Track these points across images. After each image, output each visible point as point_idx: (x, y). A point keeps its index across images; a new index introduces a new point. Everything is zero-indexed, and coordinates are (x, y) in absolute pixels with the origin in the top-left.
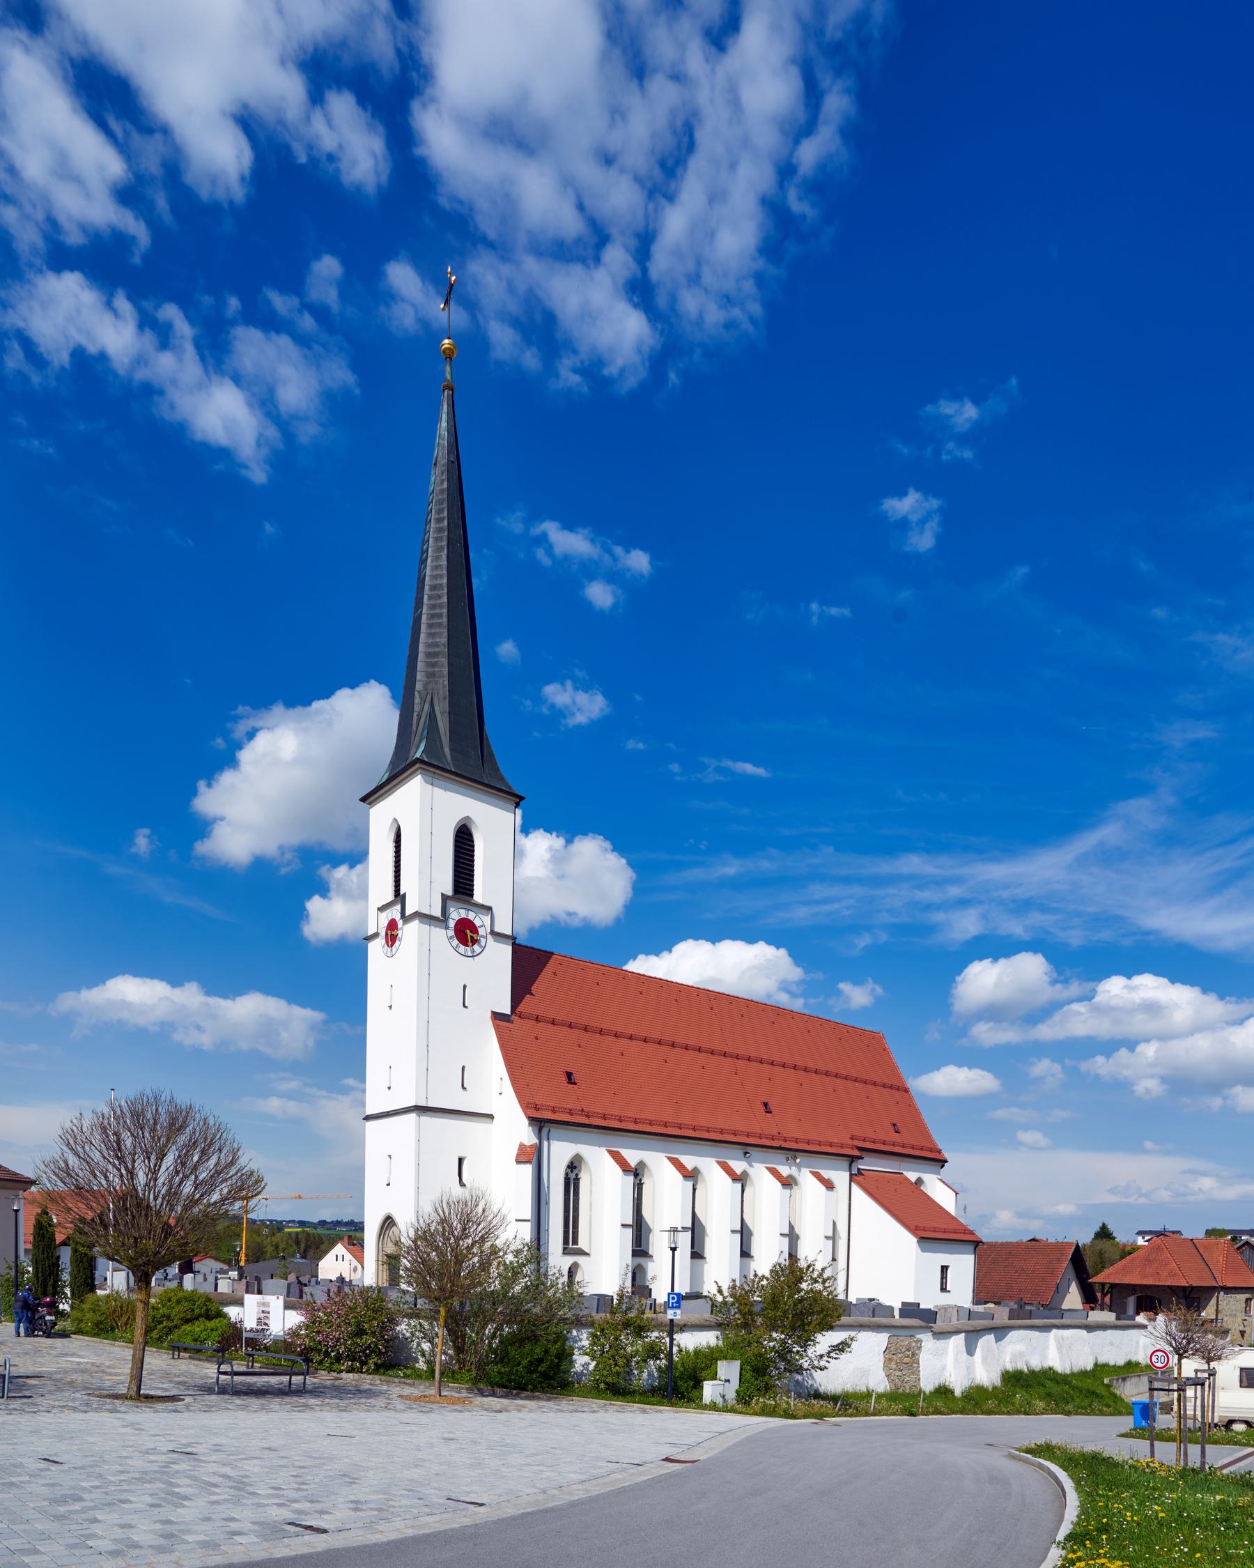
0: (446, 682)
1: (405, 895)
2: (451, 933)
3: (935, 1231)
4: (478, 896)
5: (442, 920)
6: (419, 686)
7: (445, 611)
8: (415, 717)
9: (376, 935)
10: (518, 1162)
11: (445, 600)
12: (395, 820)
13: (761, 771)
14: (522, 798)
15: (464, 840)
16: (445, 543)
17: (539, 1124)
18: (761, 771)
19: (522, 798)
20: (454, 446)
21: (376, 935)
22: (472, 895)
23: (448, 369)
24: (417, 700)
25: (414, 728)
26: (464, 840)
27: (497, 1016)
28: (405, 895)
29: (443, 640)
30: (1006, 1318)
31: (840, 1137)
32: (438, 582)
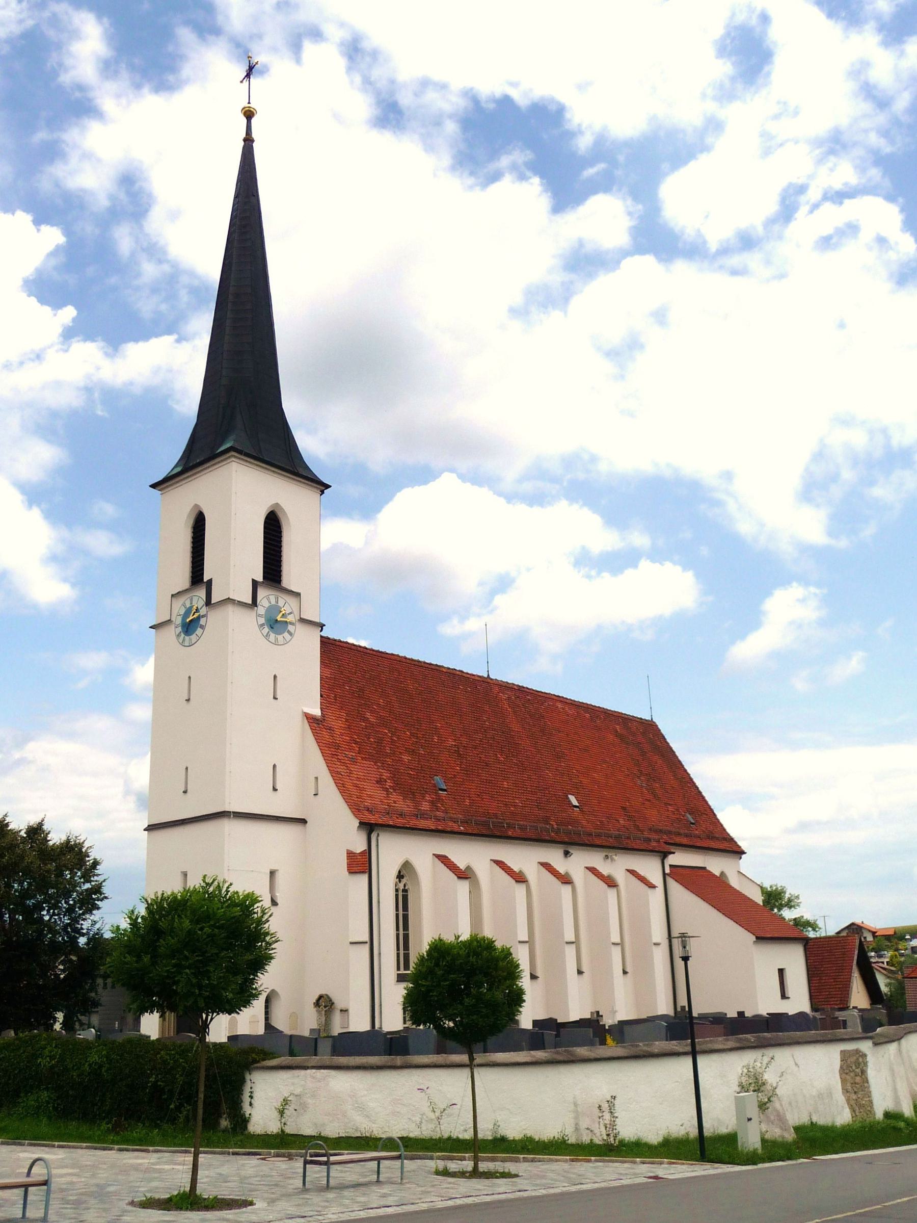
2: (262, 621)
17: (369, 828)
27: (310, 718)
28: (210, 582)
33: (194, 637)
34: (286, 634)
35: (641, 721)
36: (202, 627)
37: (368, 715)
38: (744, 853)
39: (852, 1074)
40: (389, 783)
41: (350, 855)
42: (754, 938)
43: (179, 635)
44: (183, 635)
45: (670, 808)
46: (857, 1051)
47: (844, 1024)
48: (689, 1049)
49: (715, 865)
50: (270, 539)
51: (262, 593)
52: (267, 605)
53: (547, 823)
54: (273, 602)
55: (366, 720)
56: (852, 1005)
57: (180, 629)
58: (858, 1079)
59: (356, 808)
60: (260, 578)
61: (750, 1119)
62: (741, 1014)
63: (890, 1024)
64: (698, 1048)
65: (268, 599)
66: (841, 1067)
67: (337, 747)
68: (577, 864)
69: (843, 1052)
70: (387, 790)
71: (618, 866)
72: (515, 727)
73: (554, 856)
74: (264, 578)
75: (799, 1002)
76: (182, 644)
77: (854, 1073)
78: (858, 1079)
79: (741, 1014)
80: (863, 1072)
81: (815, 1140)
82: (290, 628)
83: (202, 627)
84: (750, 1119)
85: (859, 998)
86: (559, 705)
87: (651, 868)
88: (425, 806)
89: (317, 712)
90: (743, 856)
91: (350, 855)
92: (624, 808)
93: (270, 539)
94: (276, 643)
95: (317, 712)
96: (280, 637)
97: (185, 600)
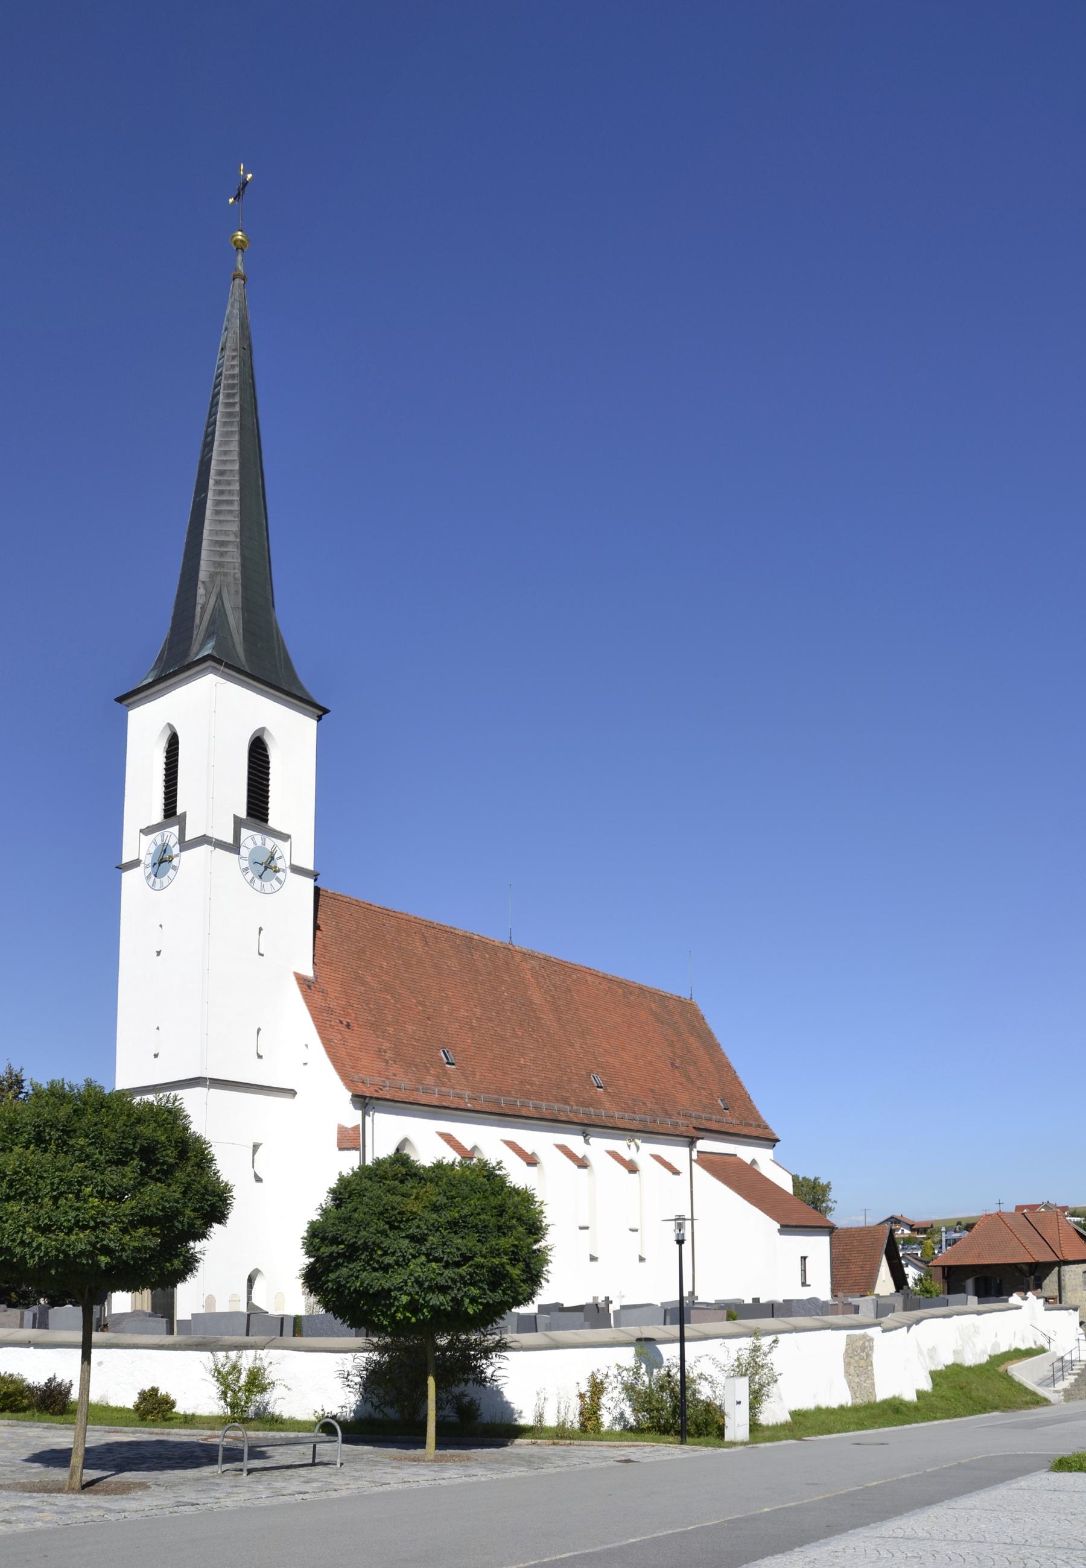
0: (239, 576)
1: (184, 815)
2: (245, 864)
3: (801, 1209)
4: (274, 821)
5: (234, 847)
6: (203, 575)
7: (236, 498)
8: (198, 609)
9: (136, 863)
10: (341, 1149)
11: (236, 487)
12: (170, 726)
13: (431, 1382)
14: (326, 711)
15: (258, 753)
16: (236, 428)
17: (364, 1102)
18: (431, 1382)
19: (326, 711)
20: (244, 326)
21: (136, 863)
22: (266, 821)
23: (240, 258)
24: (201, 591)
25: (197, 621)
26: (258, 753)
27: (301, 980)
28: (184, 815)
29: (235, 527)
30: (873, 1315)
31: (683, 1125)
32: (228, 467)
33: (165, 879)
34: (274, 882)
35: (679, 1000)
36: (175, 868)
37: (368, 978)
38: (778, 1141)
39: (856, 1358)
40: (389, 1055)
41: (342, 1131)
42: (779, 1226)
43: (148, 877)
44: (153, 877)
45: (703, 1093)
46: (864, 1336)
47: (857, 1309)
48: (678, 1334)
49: (746, 1153)
50: (255, 763)
51: (245, 833)
52: (252, 846)
53: (566, 1102)
54: (259, 843)
55: (364, 983)
56: (876, 1292)
57: (149, 870)
58: (862, 1363)
59: (348, 1080)
60: (243, 813)
61: (739, 1403)
62: (756, 1300)
63: (905, 1309)
64: (686, 1334)
65: (253, 840)
66: (846, 1351)
67: (330, 1011)
68: (597, 1148)
69: (850, 1341)
70: (387, 1062)
71: (643, 1152)
72: (537, 998)
73: (575, 1142)
74: (249, 814)
75: (821, 1288)
76: (152, 887)
77: (858, 1360)
78: (862, 1363)
79: (756, 1300)
80: (869, 1356)
81: (806, 1423)
82: (280, 875)
83: (175, 868)
84: (739, 1403)
85: (885, 1283)
86: (589, 978)
87: (677, 1155)
88: (429, 1080)
89: (308, 972)
90: (777, 1144)
91: (342, 1131)
92: (653, 1091)
93: (255, 763)
94: (262, 891)
95: (308, 972)
96: (267, 885)
97: (157, 836)
